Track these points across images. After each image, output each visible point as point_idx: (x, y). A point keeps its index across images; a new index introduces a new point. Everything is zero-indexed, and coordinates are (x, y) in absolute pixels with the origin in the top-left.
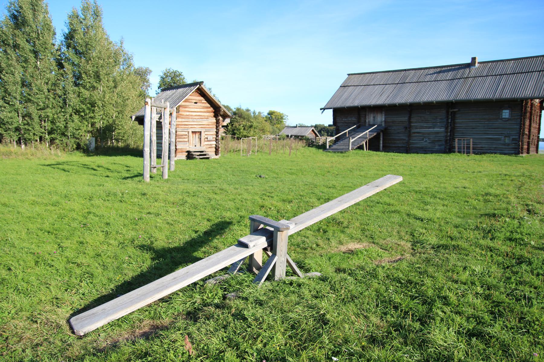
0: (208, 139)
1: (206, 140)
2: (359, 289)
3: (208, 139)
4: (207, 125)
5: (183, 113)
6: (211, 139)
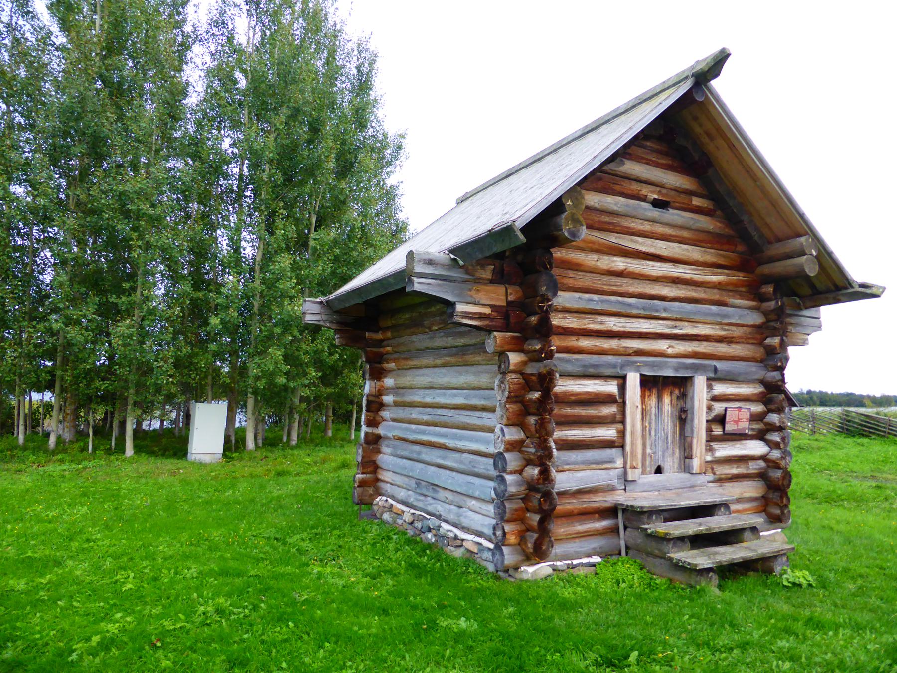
0: (730, 427)
1: (717, 431)
2: (219, 89)
3: (730, 427)
5: (590, 259)
6: (745, 426)
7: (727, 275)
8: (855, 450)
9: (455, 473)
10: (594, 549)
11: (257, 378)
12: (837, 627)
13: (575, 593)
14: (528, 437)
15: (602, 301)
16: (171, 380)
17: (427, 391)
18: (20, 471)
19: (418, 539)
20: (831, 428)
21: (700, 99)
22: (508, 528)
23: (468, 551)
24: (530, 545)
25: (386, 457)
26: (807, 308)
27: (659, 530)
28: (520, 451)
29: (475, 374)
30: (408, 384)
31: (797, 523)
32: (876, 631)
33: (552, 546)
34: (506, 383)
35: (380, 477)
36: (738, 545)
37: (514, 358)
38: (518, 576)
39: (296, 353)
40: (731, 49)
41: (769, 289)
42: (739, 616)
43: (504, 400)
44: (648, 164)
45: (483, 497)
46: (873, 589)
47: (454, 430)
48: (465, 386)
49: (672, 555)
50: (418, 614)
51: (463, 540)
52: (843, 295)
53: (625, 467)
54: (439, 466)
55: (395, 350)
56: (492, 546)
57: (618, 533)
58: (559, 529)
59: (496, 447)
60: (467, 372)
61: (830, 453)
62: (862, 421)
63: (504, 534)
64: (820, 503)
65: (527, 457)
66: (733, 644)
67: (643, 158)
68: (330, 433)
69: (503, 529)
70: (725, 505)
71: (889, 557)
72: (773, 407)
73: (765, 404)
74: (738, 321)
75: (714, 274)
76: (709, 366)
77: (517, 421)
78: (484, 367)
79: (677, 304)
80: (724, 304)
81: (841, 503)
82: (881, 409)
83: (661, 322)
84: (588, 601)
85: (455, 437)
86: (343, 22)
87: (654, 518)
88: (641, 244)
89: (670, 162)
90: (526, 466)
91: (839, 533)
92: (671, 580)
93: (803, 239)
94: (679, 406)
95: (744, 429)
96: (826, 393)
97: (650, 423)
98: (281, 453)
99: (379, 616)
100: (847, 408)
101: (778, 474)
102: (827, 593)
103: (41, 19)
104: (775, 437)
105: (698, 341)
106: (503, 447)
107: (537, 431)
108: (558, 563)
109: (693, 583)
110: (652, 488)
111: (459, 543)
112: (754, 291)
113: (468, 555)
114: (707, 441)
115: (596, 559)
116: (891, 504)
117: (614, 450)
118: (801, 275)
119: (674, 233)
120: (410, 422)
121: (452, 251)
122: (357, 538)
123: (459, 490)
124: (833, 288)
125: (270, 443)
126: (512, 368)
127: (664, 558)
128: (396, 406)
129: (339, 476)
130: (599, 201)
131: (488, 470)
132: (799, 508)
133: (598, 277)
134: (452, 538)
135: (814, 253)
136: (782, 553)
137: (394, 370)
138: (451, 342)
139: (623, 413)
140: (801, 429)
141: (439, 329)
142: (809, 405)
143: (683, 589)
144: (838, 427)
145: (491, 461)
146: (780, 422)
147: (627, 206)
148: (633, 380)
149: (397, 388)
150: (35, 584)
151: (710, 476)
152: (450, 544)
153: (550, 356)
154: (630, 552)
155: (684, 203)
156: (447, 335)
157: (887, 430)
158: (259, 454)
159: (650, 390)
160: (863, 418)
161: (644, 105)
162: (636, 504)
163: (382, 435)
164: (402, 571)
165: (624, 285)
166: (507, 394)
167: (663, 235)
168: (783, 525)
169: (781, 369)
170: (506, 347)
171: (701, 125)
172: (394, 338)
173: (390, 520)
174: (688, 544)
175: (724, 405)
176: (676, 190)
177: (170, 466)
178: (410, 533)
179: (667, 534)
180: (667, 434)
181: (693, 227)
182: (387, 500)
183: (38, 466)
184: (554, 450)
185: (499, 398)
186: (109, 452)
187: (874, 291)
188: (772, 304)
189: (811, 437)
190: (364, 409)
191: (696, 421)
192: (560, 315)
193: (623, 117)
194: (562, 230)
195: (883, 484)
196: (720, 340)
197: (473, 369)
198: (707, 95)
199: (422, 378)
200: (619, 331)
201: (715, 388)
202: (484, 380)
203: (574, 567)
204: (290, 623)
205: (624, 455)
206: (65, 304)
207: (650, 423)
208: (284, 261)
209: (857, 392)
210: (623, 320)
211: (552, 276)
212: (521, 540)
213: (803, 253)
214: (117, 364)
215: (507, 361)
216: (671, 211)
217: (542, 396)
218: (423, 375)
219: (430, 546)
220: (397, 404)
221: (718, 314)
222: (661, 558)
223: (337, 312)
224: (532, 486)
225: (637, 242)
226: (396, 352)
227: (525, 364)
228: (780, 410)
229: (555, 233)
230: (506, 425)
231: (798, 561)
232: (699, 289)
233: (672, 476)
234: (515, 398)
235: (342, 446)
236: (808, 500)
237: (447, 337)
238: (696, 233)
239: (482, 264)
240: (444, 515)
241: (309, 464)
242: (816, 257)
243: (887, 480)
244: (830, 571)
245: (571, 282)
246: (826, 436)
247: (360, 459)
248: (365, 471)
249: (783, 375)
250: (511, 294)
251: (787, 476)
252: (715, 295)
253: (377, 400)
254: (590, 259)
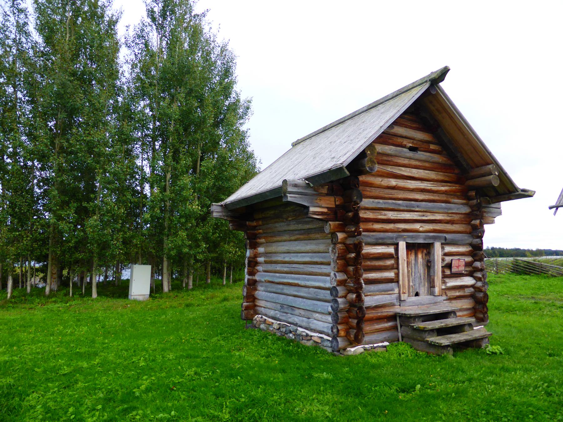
0: (454, 270)
1: (448, 272)
3: (454, 270)
5: (378, 181)
6: (462, 269)
7: (450, 186)
8: (522, 282)
9: (305, 300)
10: (385, 338)
11: (170, 249)
12: (515, 370)
13: (378, 361)
14: (348, 278)
15: (385, 203)
16: (121, 251)
17: (285, 255)
18: (31, 308)
19: (284, 337)
20: (507, 270)
21: (434, 93)
22: (340, 327)
23: (315, 342)
24: (352, 336)
25: (260, 292)
26: (493, 203)
27: (420, 326)
28: (345, 286)
29: (316, 244)
30: (273, 251)
31: (491, 323)
32: (536, 371)
33: (364, 337)
34: (337, 249)
35: (257, 304)
36: (462, 333)
37: (340, 236)
38: (345, 353)
39: (194, 234)
40: (450, 67)
41: (473, 193)
42: (466, 368)
43: (336, 258)
44: (406, 127)
45: (323, 311)
46: (534, 354)
47: (303, 276)
48: (310, 251)
49: (428, 339)
50: (301, 372)
51: (311, 336)
52: (513, 196)
53: (399, 293)
54: (295, 296)
55: (265, 231)
56: (330, 339)
57: (397, 329)
58: (367, 328)
59: (331, 284)
60: (311, 244)
61: (507, 285)
62: (525, 265)
63: (338, 331)
64: (503, 313)
65: (349, 289)
66: (464, 380)
67: (403, 124)
68: (209, 281)
69: (337, 328)
70: (454, 312)
71: (542, 338)
72: (477, 258)
73: (473, 257)
74: (457, 212)
75: (443, 186)
76: (442, 237)
77: (343, 269)
78: (321, 240)
79: (424, 203)
80: (449, 203)
81: (515, 312)
82: (537, 258)
83: (416, 213)
84: (385, 364)
85: (305, 279)
86: (214, 36)
88: (404, 171)
89: (418, 126)
90: (348, 294)
91: (515, 327)
92: (428, 353)
93: (490, 166)
94: (427, 259)
95: (462, 271)
96: (503, 249)
97: (411, 269)
98: (185, 294)
99: (281, 373)
100: (516, 258)
101: (481, 295)
102: (510, 357)
103: (31, 35)
104: (479, 275)
105: (436, 223)
106: (336, 284)
107: (354, 274)
108: (367, 346)
109: (440, 354)
110: (414, 304)
111: (309, 338)
112: (464, 195)
113: (315, 344)
114: (442, 278)
115: (386, 343)
116: (543, 312)
117: (393, 284)
118: (490, 185)
119: (421, 165)
120: (276, 272)
121: (306, 179)
122: (248, 339)
123: (308, 309)
124: (508, 192)
125: (176, 287)
126: (339, 241)
127: (424, 341)
128: (265, 263)
129: (225, 306)
130: (381, 149)
131: (326, 297)
132: (492, 315)
133: (382, 190)
134: (304, 335)
135: (497, 174)
136: (485, 336)
137: (264, 243)
138: (300, 227)
139: (397, 263)
140: (489, 271)
141: (293, 219)
142: (493, 257)
143: (434, 357)
144: (511, 269)
145: (329, 292)
146: (481, 266)
147: (396, 151)
148: (402, 245)
149: (266, 253)
150: (91, 364)
151: (444, 297)
152: (304, 339)
153: (360, 234)
154: (404, 339)
155: (425, 148)
156: (298, 223)
157: (540, 270)
158: (171, 294)
159: (411, 250)
160: (525, 263)
161: (403, 95)
162: (406, 313)
163: (258, 280)
164: (281, 354)
165: (396, 194)
166: (337, 255)
167: (415, 166)
168: (484, 323)
169: (481, 237)
170: (336, 230)
171: (434, 106)
172: (263, 225)
173: (265, 328)
174: (436, 333)
175: (451, 258)
176: (421, 141)
177: (121, 303)
178: (279, 334)
179: (425, 328)
180: (421, 274)
181: (431, 161)
182: (262, 317)
183: (42, 305)
184: (363, 284)
185: (332, 257)
186: (81, 296)
187: (529, 193)
188: (475, 202)
189: (496, 276)
190: (247, 266)
191: (436, 267)
192: (363, 211)
193: (391, 102)
194: (365, 167)
195: (538, 301)
196: (447, 222)
197: (315, 242)
198: (437, 91)
199: (283, 247)
200: (394, 219)
201: (445, 248)
202: (322, 248)
203: (375, 348)
204: (238, 377)
205: (399, 286)
206: (57, 208)
207: (411, 269)
208: (186, 180)
209: (522, 248)
210: (396, 213)
211: (359, 191)
212: (347, 334)
213: (490, 174)
214: (90, 243)
215: (336, 237)
216: (419, 152)
217: (356, 256)
218: (283, 246)
219: (292, 341)
220: (266, 262)
221: (446, 208)
222: (421, 341)
223: (231, 211)
224: (352, 304)
225: (401, 170)
226: (264, 233)
227: (346, 238)
228: (481, 260)
229: (362, 168)
230: (337, 272)
231: (494, 342)
232: (435, 194)
233: (424, 297)
234: (342, 257)
235: (220, 289)
236: (496, 311)
237: (298, 224)
238: (431, 164)
239: (322, 186)
240: (299, 323)
241: (204, 300)
242: (498, 176)
243: (540, 299)
244: (511, 346)
245: (368, 194)
246: (504, 274)
247: (245, 294)
248: (248, 301)
249: (482, 241)
250: (337, 201)
251: (486, 296)
252: (443, 197)
253: (254, 260)
254: (378, 181)
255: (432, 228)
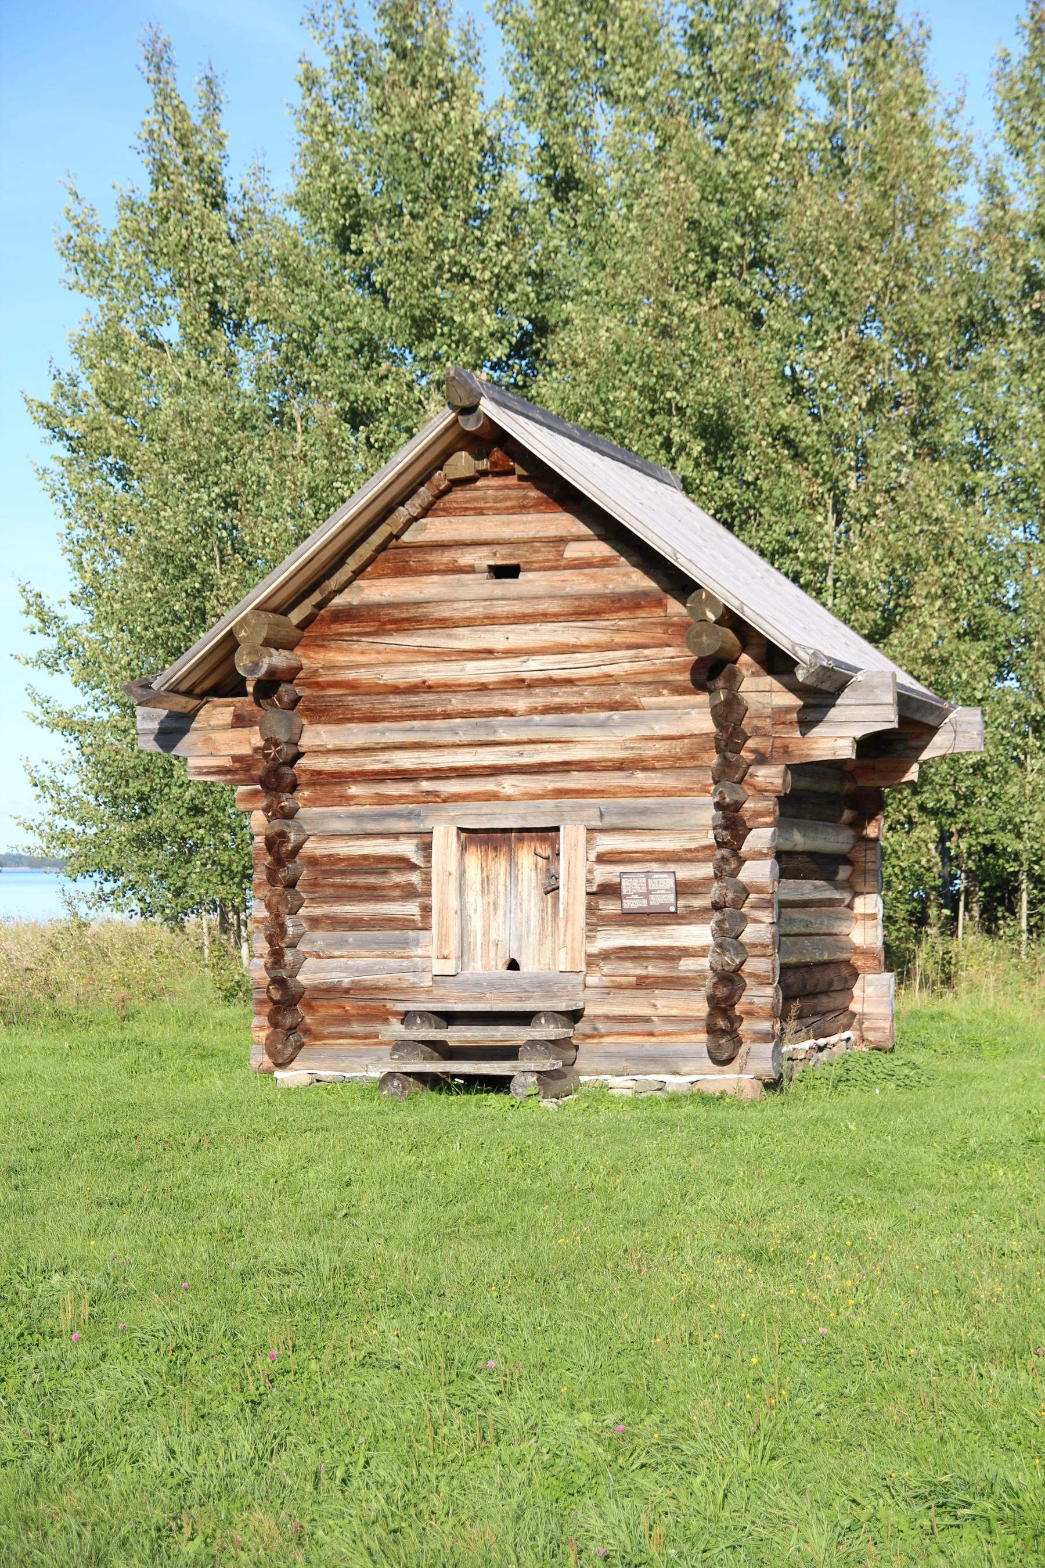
3: (631, 904)
4: (620, 766)
87: (543, 1021)
201: (599, 842)
255: (550, 786)
